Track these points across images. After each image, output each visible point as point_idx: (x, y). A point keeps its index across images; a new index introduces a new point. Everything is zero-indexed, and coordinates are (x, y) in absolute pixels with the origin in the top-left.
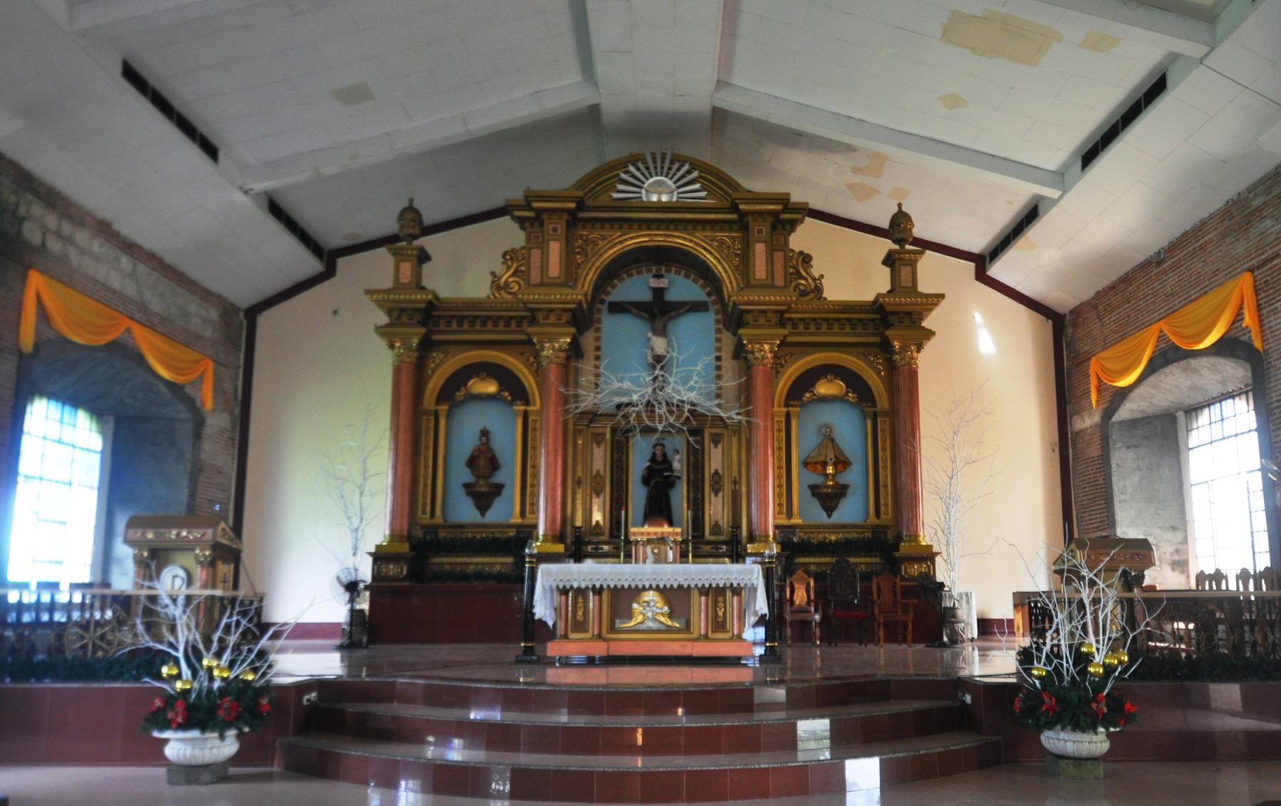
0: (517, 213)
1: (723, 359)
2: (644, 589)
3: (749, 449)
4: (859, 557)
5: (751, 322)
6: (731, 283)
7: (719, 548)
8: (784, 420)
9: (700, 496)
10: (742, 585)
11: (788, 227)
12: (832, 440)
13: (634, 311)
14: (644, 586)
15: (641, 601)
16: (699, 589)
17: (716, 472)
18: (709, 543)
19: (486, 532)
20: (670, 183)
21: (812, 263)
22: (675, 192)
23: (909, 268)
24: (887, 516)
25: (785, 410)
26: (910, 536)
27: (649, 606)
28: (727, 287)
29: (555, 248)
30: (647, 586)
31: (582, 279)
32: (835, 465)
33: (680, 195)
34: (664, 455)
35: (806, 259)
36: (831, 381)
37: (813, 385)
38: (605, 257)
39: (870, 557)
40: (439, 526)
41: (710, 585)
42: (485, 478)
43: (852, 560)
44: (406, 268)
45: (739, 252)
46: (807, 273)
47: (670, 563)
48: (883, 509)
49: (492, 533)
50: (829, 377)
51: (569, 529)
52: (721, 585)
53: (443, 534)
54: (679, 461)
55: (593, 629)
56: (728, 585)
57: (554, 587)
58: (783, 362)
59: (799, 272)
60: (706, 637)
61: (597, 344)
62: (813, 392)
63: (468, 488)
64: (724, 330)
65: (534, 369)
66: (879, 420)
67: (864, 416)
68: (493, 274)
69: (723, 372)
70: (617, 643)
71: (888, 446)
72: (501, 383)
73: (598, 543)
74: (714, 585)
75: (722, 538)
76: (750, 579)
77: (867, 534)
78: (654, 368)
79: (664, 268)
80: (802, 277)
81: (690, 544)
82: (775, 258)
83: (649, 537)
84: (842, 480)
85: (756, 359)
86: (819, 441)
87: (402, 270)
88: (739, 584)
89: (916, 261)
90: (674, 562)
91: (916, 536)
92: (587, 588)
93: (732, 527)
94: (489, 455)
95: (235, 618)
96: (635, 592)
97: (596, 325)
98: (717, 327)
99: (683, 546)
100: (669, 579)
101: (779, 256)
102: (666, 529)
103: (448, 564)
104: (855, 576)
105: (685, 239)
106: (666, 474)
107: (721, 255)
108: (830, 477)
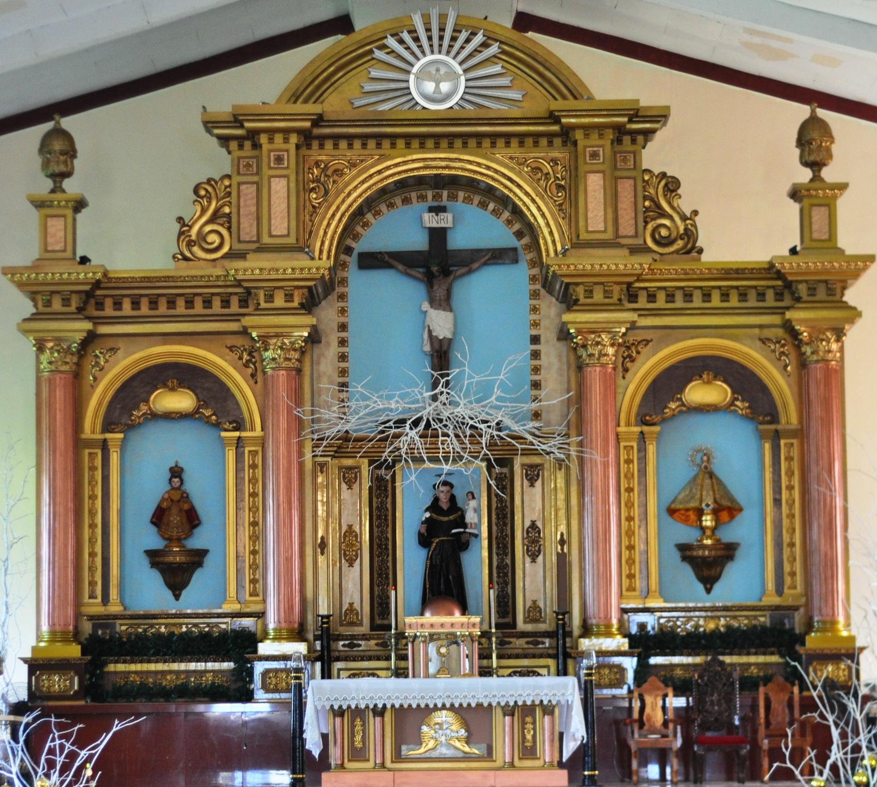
0: (216, 131)
1: (542, 339)
2: (436, 708)
3: (581, 494)
4: (748, 654)
5: (582, 300)
6: (551, 233)
7: (538, 643)
8: (635, 445)
9: (508, 561)
10: (554, 703)
11: (640, 139)
12: (711, 475)
13: (401, 267)
14: (435, 705)
15: (432, 723)
16: (503, 708)
17: (533, 525)
18: (524, 635)
19: (187, 624)
20: (455, 64)
21: (679, 191)
22: (463, 79)
23: (824, 210)
24: (793, 594)
25: (637, 429)
26: (824, 622)
27: (441, 729)
28: (544, 238)
29: (279, 188)
30: (439, 705)
31: (321, 232)
32: (716, 512)
33: (471, 84)
34: (452, 499)
35: (672, 186)
36: (709, 382)
37: (681, 390)
38: (354, 195)
39: (764, 654)
40: (116, 617)
41: (516, 702)
42: (179, 540)
43: (727, 659)
44: (56, 227)
45: (563, 183)
46: (672, 207)
47: (465, 675)
48: (788, 580)
49: (195, 625)
50: (705, 376)
51: (310, 617)
52: (529, 703)
53: (124, 628)
54: (475, 510)
55: (374, 757)
56: (537, 702)
57: (328, 707)
58: (634, 354)
59: (658, 206)
60: (512, 765)
61: (342, 320)
62: (681, 399)
63: (154, 557)
64: (543, 292)
65: (249, 371)
66: (782, 442)
67: (762, 436)
68: (180, 219)
69: (544, 361)
70: (404, 773)
71: (796, 481)
72: (203, 402)
73: (353, 637)
74: (520, 703)
75: (543, 627)
76: (563, 695)
77: (762, 619)
78: (435, 385)
79: (445, 193)
80: (664, 215)
81: (494, 639)
82: (619, 189)
83: (433, 631)
84: (728, 535)
85: (591, 356)
86: (693, 474)
87: (50, 230)
88: (550, 701)
89: (835, 197)
90: (471, 674)
91: (830, 624)
92: (533, 705)
93: (557, 614)
94: (186, 507)
95: (58, 742)
96: (426, 712)
97: (339, 290)
98: (533, 287)
99: (483, 640)
100: (465, 697)
101: (626, 189)
102: (457, 617)
103: (136, 672)
104: (732, 684)
105: (479, 165)
106: (454, 531)
107: (534, 189)
108: (708, 533)
